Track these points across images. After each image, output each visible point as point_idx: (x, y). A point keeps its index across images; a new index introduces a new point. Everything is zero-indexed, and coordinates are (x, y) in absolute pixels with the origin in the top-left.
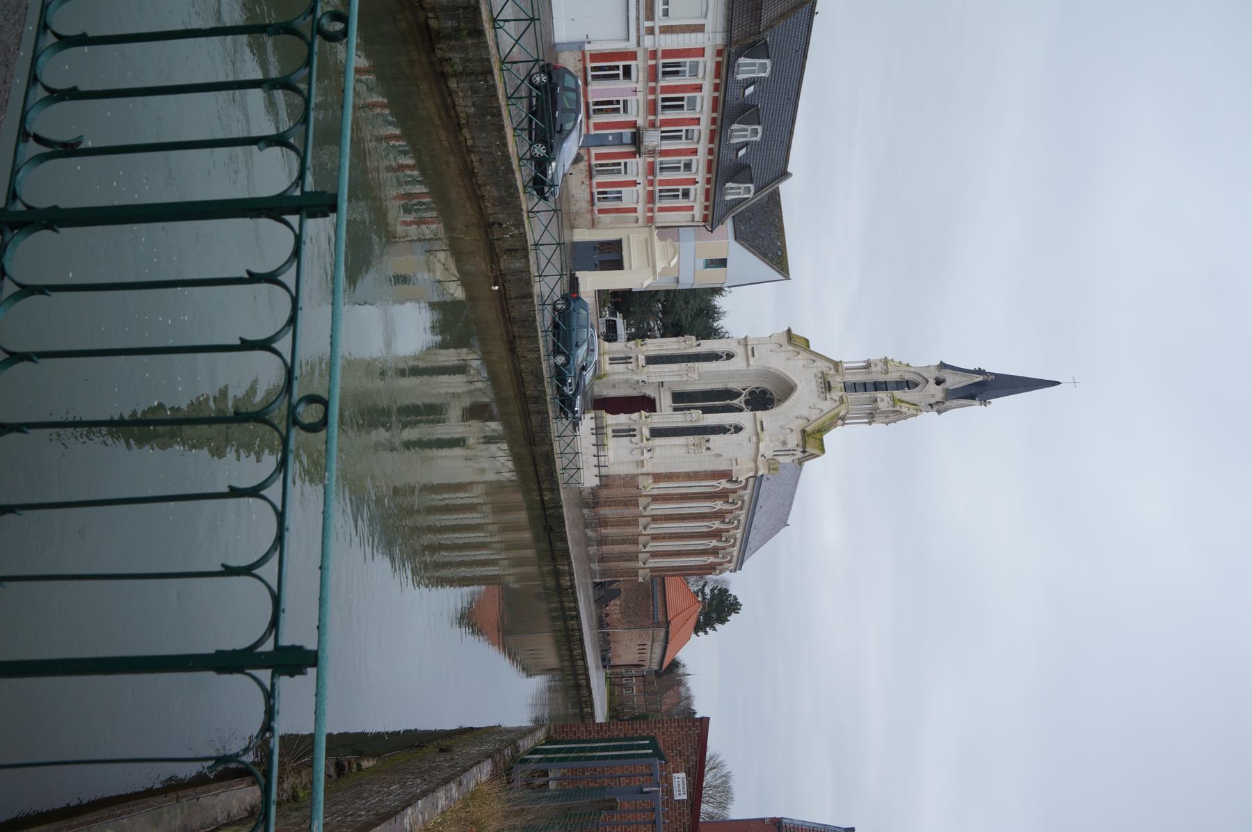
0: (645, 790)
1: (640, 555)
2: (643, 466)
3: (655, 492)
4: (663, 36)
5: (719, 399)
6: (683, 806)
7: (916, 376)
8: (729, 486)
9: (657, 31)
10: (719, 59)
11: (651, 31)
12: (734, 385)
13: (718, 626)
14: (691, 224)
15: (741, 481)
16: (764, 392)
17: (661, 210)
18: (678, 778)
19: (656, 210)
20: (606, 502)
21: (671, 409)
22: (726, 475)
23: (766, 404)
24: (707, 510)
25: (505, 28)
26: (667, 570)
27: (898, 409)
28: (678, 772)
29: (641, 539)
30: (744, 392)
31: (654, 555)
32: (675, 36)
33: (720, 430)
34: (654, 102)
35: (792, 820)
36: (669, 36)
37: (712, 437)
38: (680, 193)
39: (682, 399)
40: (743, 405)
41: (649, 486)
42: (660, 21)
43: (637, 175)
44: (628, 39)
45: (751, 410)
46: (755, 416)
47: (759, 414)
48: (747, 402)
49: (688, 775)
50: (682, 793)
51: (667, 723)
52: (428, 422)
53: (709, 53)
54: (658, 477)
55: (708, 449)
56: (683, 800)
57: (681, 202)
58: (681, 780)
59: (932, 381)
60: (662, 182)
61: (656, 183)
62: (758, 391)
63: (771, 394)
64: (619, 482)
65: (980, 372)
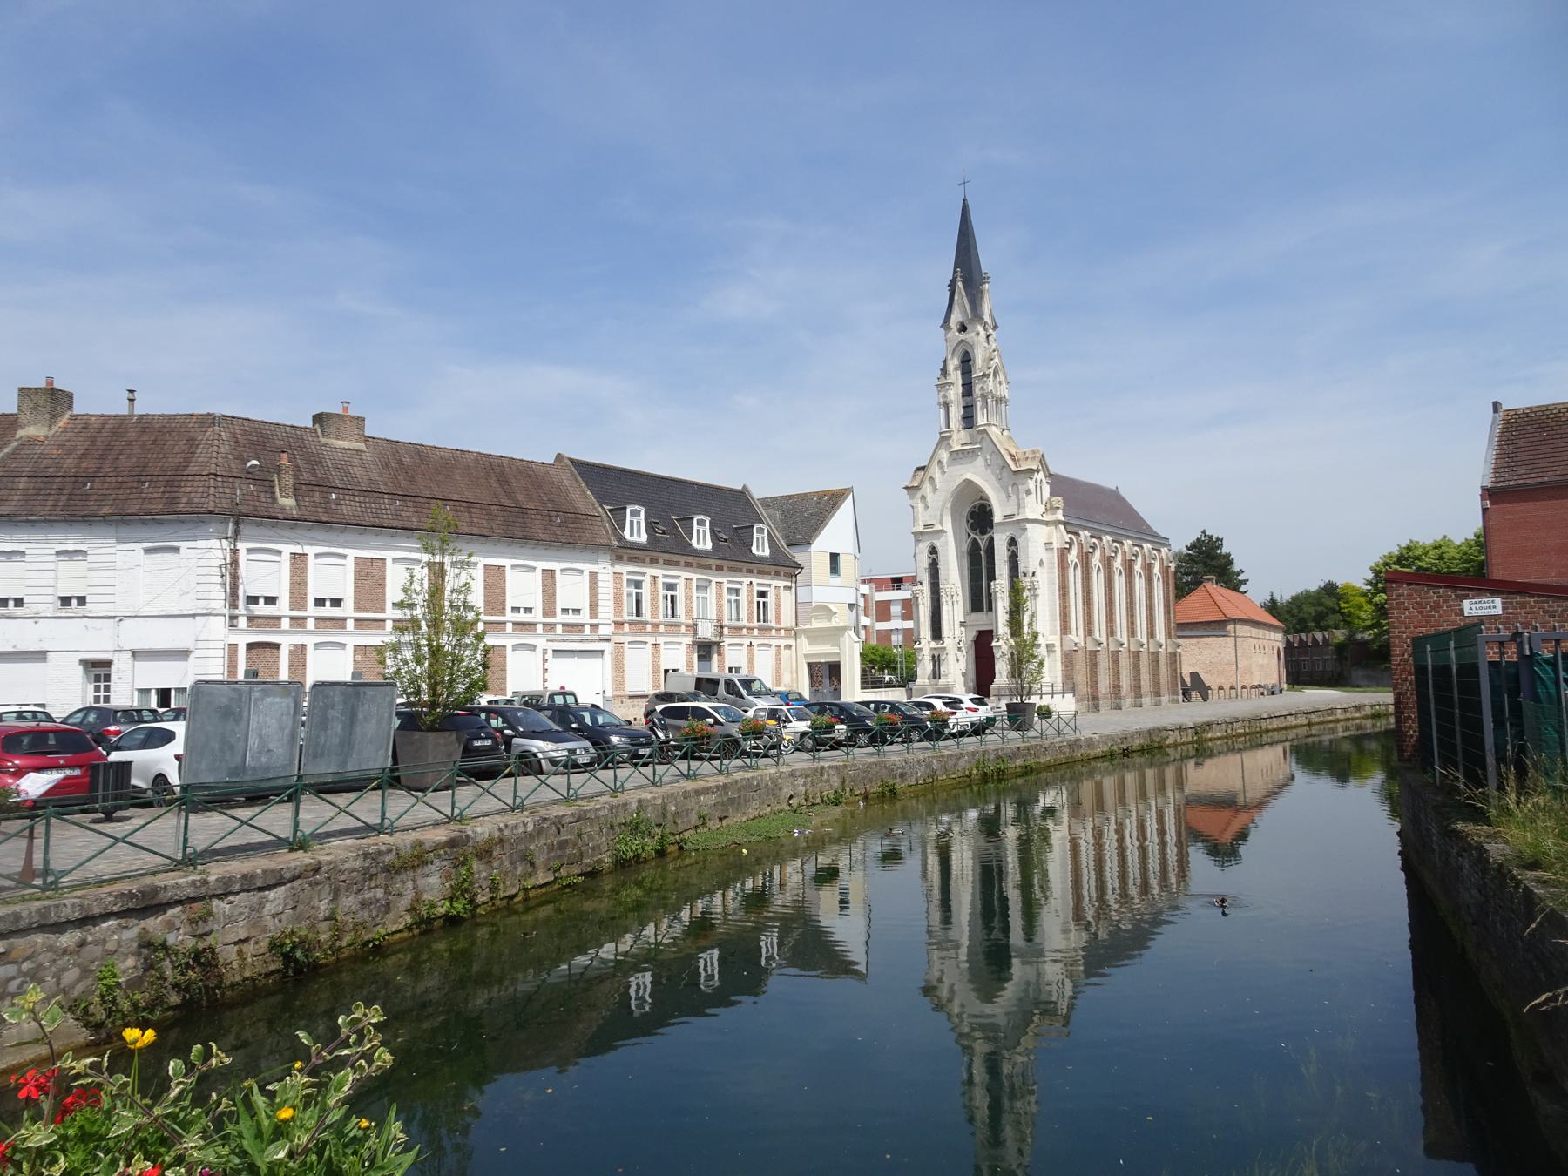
0: (1528, 653)
1: (1151, 650)
2: (1053, 645)
3: (1081, 632)
4: (600, 616)
5: (979, 565)
6: (1511, 603)
7: (944, 518)
8: (1074, 551)
9: (595, 621)
10: (625, 558)
11: (595, 626)
12: (965, 547)
13: (1236, 568)
14: (793, 589)
15: (1070, 538)
16: (972, 515)
17: (778, 620)
18: (1471, 609)
19: (778, 626)
20: (1092, 687)
21: (990, 613)
22: (1063, 554)
23: (985, 512)
24: (1102, 575)
25: (577, 786)
26: (1169, 620)
27: (992, 370)
28: (1463, 610)
29: (1091, 647)
30: (972, 535)
31: (1151, 634)
32: (600, 603)
33: (1013, 560)
34: (760, 629)
35: (1483, 476)
36: (600, 609)
37: (1021, 569)
38: (762, 600)
39: (979, 600)
40: (986, 537)
41: (1077, 636)
42: (584, 617)
43: (742, 645)
44: (602, 651)
45: (992, 527)
46: (1000, 524)
47: (997, 518)
48: (983, 533)
49: (1467, 597)
50: (1492, 605)
51: (1394, 622)
52: (1000, 879)
53: (618, 568)
54: (1065, 629)
55: (1034, 574)
56: (1503, 603)
57: (771, 599)
58: (1473, 606)
59: (962, 336)
60: (750, 619)
61: (751, 625)
62: (971, 521)
63: (974, 507)
64: (220, 459)
65: (952, 286)
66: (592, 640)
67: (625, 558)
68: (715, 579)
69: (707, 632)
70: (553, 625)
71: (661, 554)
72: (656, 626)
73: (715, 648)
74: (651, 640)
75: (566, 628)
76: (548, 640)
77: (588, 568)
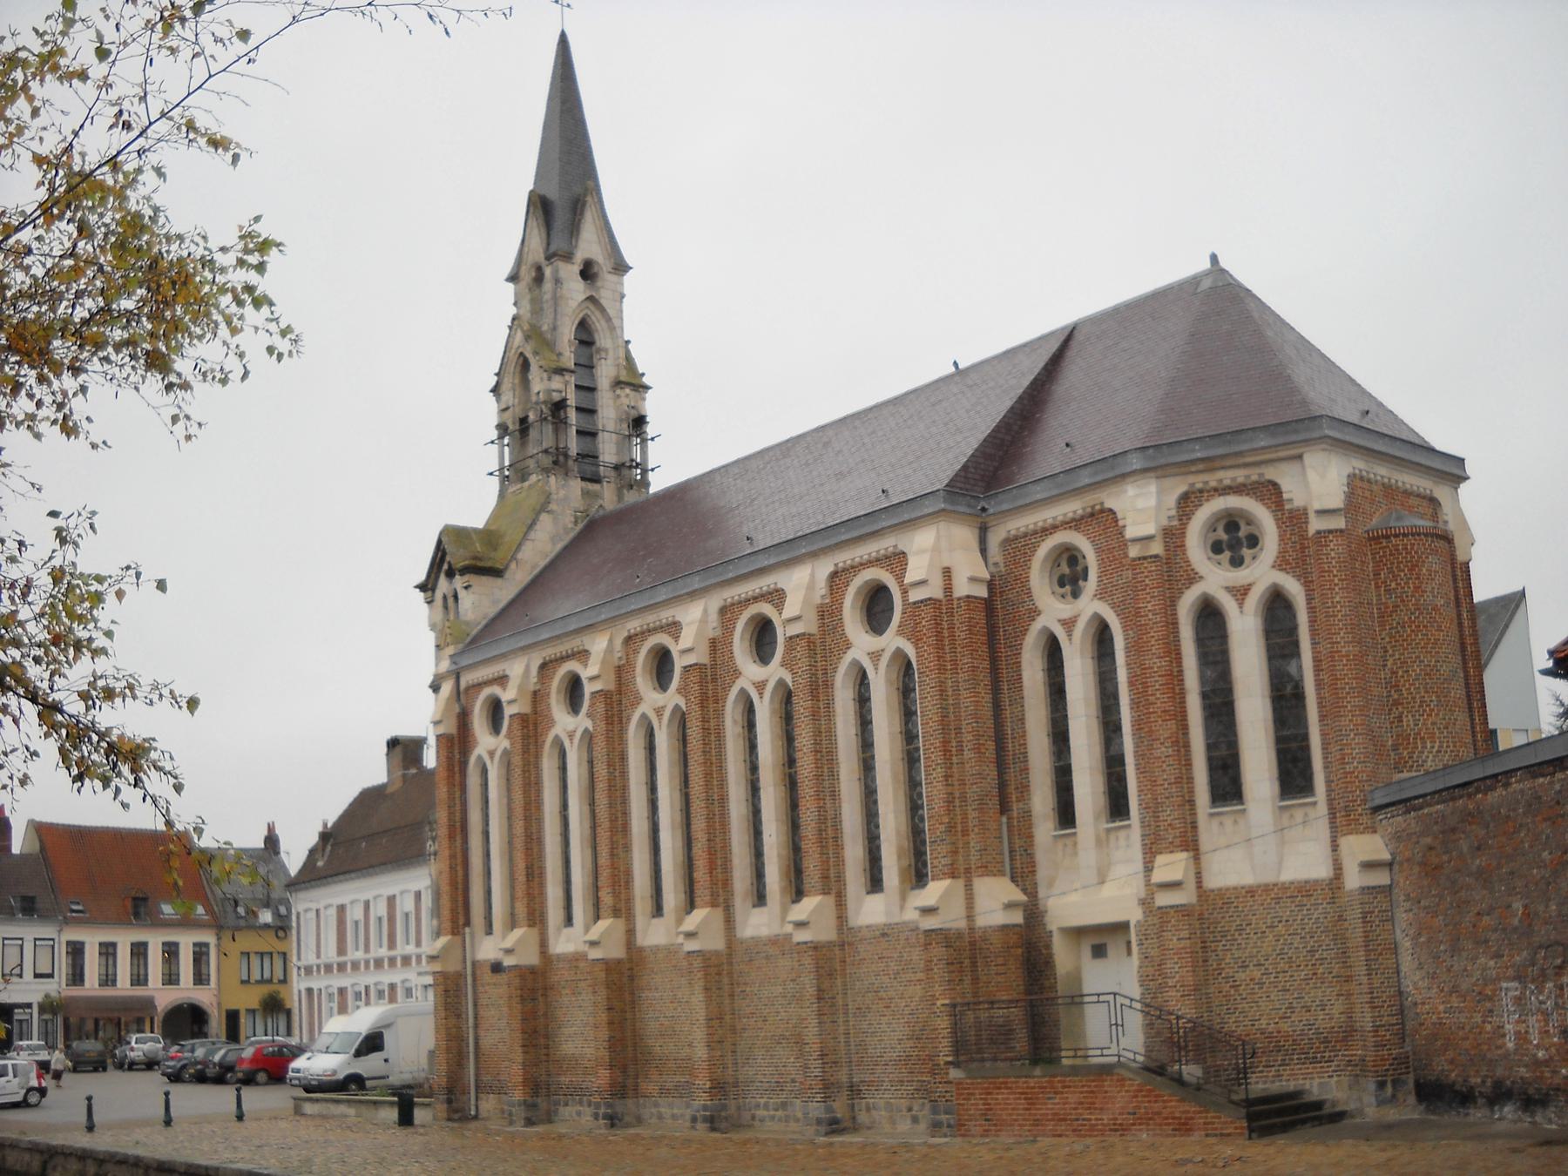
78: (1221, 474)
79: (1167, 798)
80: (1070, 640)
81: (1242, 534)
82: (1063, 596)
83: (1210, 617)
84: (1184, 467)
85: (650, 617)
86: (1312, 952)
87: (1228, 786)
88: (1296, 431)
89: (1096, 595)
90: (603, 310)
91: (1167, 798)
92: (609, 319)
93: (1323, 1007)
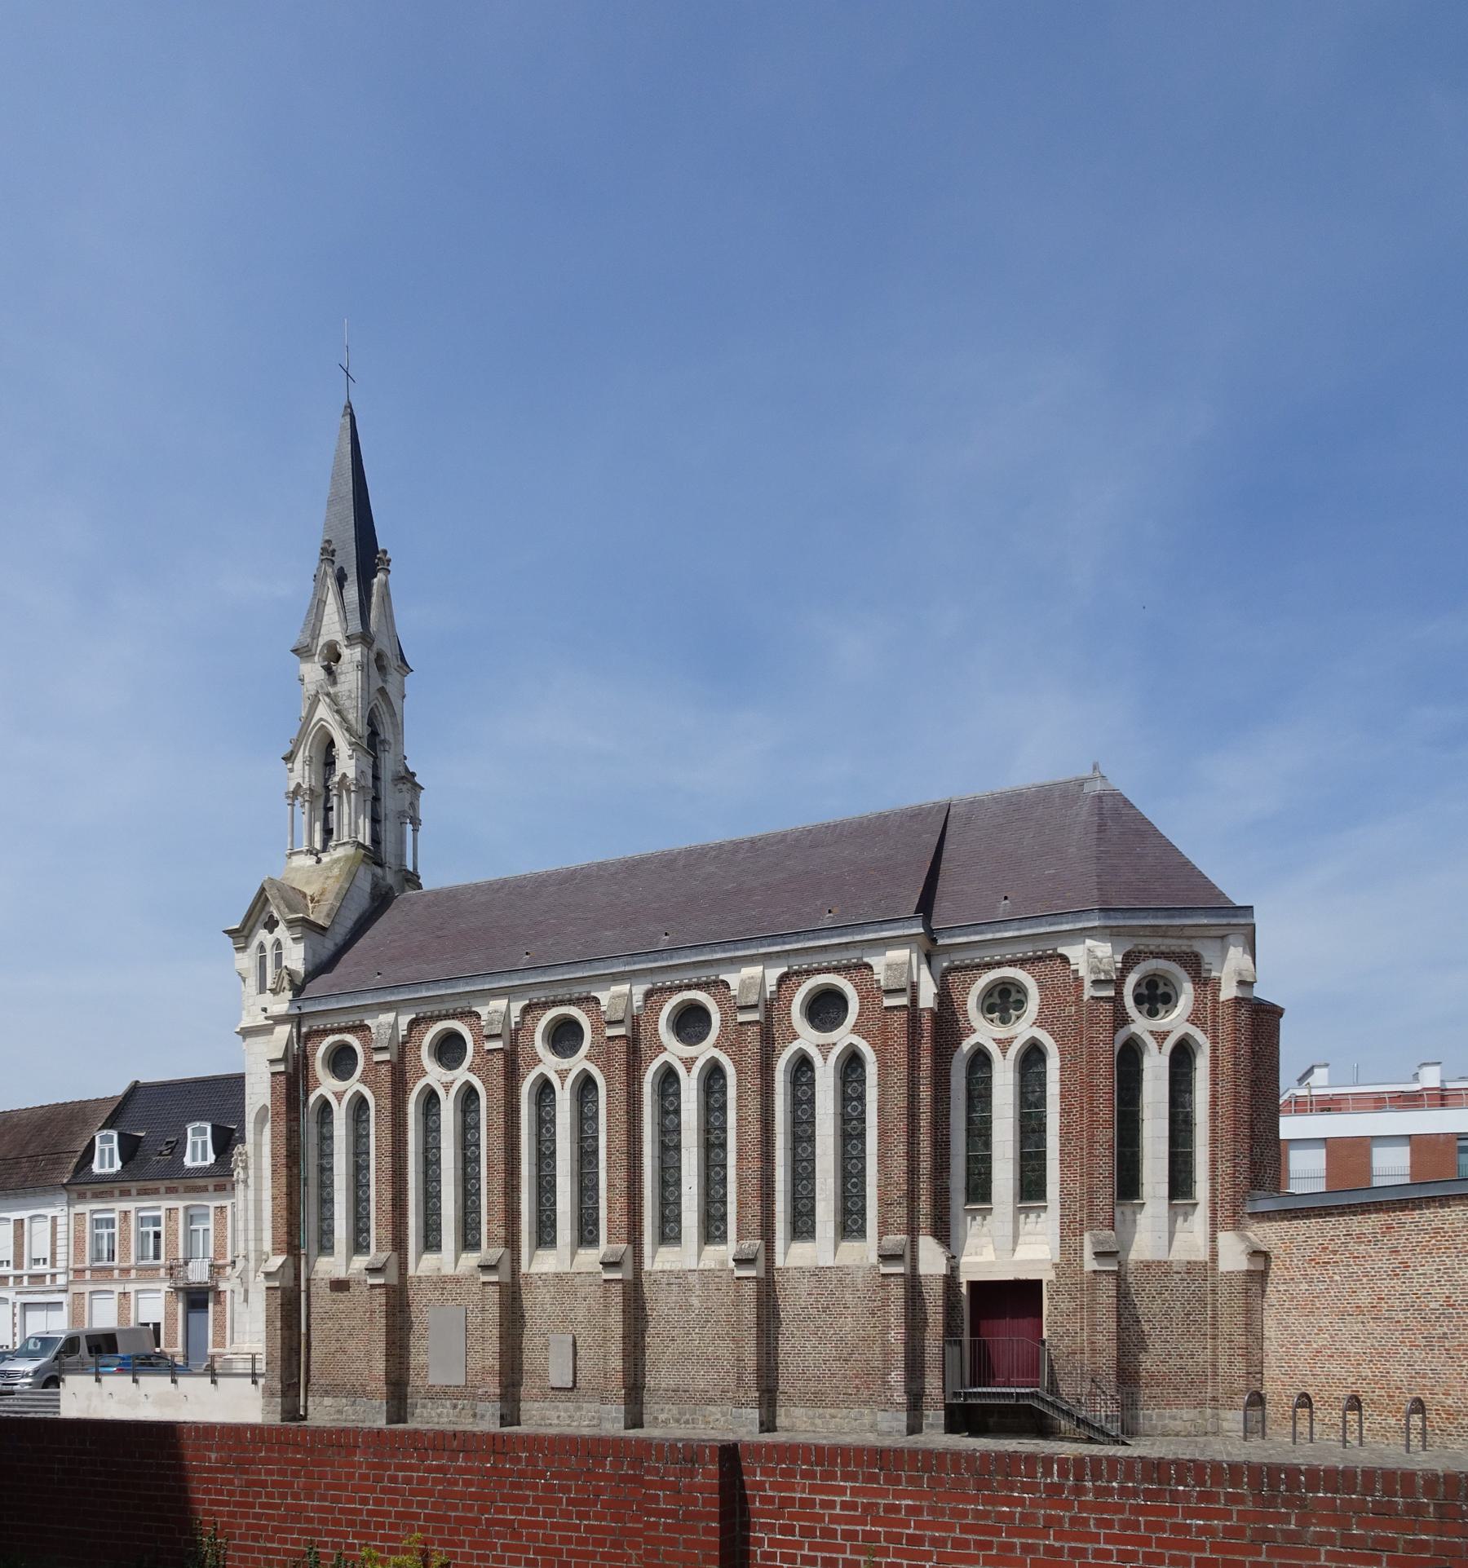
9: (54, 1271)
66: (52, 1292)
67: (89, 1194)
68: (213, 1204)
69: (198, 1273)
70: (21, 1277)
71: (134, 1184)
72: (125, 1271)
73: (211, 1296)
74: (118, 1288)
75: (33, 1280)
76: (17, 1293)
77: (50, 1212)
78: (1168, 941)
79: (1101, 1188)
80: (1004, 1056)
81: (1159, 992)
82: (992, 1021)
83: (803, 1065)
84: (1131, 932)
85: (560, 990)
86: (1188, 1314)
87: (980, 1190)
88: (1236, 916)
89: (1034, 1023)
90: (389, 703)
91: (1101, 1188)
92: (393, 714)
93: (1192, 1356)
